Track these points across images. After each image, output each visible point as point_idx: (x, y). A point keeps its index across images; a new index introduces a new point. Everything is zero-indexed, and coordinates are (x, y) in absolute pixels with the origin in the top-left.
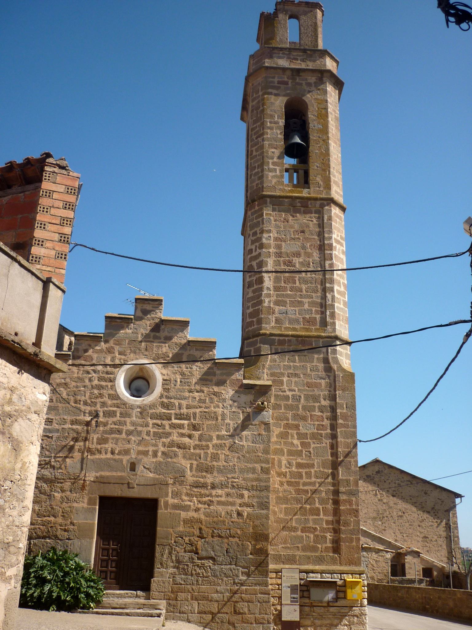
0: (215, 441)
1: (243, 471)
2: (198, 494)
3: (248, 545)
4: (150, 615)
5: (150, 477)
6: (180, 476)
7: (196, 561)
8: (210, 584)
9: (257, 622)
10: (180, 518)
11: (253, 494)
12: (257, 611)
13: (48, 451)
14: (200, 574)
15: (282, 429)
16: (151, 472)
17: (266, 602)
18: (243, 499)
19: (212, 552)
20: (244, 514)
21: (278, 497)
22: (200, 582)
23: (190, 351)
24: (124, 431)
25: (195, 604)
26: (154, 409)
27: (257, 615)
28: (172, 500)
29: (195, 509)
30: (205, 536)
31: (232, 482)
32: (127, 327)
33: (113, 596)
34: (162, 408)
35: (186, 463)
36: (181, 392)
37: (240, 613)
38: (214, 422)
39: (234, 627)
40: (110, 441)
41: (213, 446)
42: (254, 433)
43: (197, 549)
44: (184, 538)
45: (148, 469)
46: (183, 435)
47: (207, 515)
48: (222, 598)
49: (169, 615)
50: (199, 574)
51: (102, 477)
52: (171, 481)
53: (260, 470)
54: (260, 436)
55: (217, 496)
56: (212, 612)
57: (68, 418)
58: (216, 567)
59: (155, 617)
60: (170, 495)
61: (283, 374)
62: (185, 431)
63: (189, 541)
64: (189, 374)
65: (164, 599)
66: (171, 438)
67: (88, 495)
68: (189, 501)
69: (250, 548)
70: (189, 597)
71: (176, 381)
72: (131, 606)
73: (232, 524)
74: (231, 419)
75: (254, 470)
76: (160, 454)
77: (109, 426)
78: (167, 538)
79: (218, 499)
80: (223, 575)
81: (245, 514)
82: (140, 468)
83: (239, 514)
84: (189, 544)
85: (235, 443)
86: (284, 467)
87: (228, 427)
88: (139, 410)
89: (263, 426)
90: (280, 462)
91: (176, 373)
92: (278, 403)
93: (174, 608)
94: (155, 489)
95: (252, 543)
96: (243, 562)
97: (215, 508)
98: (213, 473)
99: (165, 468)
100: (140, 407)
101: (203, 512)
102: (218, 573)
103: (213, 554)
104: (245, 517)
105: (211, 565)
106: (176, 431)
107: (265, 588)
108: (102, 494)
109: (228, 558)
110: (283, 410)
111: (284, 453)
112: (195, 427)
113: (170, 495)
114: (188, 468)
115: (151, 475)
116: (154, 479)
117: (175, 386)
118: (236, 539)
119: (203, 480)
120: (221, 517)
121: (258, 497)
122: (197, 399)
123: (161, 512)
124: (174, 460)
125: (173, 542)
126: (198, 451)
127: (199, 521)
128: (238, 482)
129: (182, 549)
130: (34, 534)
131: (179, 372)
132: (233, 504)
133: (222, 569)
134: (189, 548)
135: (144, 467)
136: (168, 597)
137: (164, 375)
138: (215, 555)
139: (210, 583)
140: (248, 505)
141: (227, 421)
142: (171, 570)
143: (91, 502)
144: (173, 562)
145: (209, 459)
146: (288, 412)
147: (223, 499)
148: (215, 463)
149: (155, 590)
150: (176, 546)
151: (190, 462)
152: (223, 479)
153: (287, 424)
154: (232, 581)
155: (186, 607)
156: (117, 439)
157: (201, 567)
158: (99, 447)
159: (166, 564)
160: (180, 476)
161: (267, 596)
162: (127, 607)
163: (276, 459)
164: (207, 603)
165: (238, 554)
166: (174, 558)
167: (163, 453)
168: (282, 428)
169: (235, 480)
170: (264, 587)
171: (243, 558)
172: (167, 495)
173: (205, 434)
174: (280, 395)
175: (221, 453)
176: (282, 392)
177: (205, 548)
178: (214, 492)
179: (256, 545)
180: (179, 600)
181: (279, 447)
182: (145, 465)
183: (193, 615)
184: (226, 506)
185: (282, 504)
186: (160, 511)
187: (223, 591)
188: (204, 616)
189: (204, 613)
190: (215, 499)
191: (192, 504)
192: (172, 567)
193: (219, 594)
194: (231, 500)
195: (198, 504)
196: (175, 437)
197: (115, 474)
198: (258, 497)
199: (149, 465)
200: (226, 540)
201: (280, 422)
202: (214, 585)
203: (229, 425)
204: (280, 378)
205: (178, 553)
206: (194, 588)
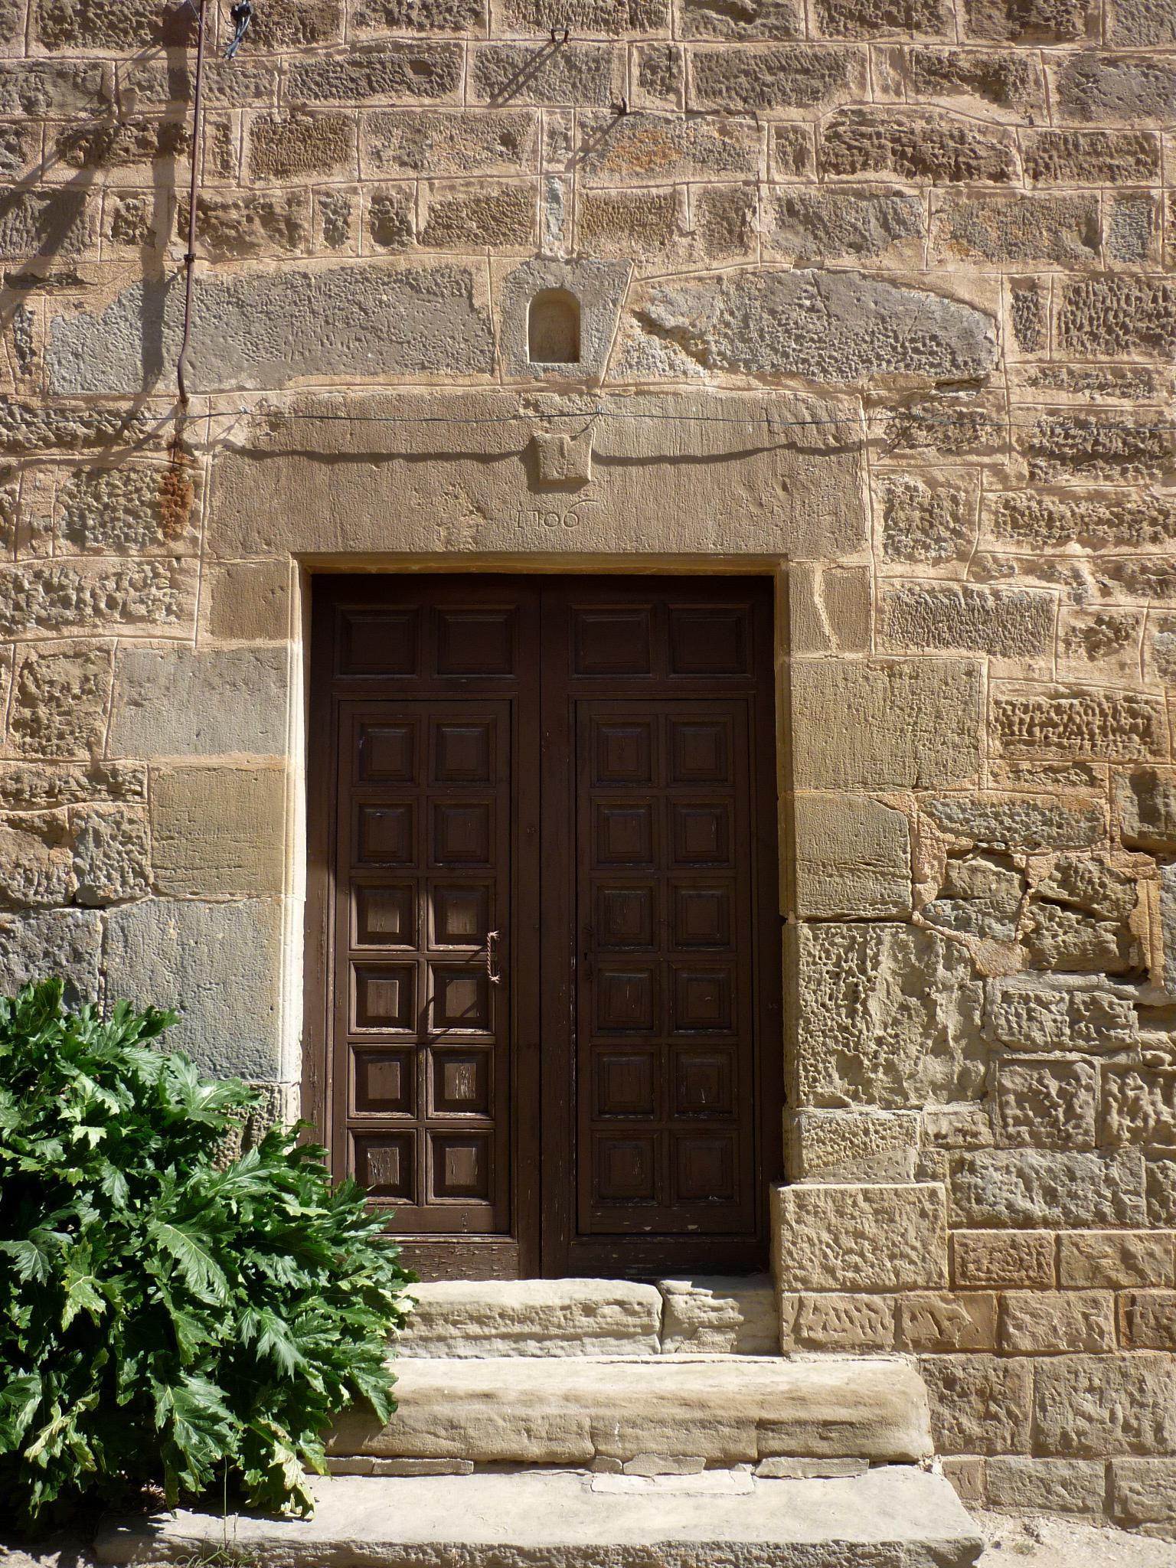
2: (1103, 512)
5: (703, 399)
6: (940, 385)
16: (702, 358)
33: (474, 1329)
52: (874, 426)
63: (1064, 883)
65: (899, 1346)
68: (1030, 569)
114: (1005, 316)
115: (711, 383)
116: (735, 411)
125: (929, 891)
135: (651, 325)
150: (963, 924)
160: (940, 385)
162: (615, 1448)
166: (949, 1018)
172: (852, 535)
191: (1058, 591)
205: (978, 975)
206: (1137, 1248)
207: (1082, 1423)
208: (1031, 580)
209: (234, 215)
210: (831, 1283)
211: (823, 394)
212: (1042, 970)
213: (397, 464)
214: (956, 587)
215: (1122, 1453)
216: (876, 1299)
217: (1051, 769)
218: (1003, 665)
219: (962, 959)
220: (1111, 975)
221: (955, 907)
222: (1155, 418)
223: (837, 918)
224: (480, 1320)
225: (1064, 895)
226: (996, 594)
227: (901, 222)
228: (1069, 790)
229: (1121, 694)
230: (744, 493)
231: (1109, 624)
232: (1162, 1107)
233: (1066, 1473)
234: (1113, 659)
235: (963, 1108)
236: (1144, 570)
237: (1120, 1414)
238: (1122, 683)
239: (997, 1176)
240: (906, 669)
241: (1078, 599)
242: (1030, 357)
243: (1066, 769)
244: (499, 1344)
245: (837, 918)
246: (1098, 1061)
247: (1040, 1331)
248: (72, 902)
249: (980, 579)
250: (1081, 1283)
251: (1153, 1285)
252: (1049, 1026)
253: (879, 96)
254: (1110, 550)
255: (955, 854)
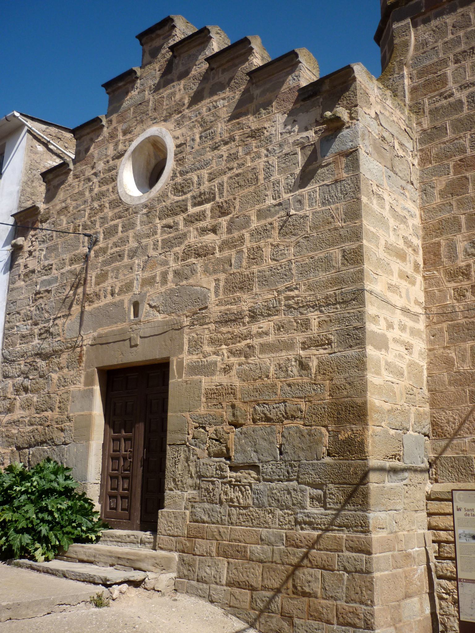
0: (255, 224)
1: (307, 269)
2: (230, 336)
3: (321, 433)
4: (91, 580)
5: (159, 321)
6: (200, 310)
7: (229, 473)
8: (252, 523)
9: (341, 620)
10: (200, 389)
11: (329, 316)
12: (342, 593)
13: (48, 312)
14: (233, 502)
15: (451, 176)
16: (159, 311)
17: (361, 572)
18: (309, 332)
19: (253, 454)
20: (311, 364)
21: (453, 326)
22: (234, 518)
23: (213, 78)
24: (126, 252)
25: (223, 563)
26: (164, 201)
27: (341, 603)
28: (190, 357)
29: (225, 368)
30: (241, 421)
31: (288, 298)
32: (133, 88)
33: (111, 539)
34: (175, 195)
35: (209, 282)
36: (201, 155)
37: (305, 594)
38: (252, 189)
39: (292, 625)
40: (110, 274)
41: (252, 235)
42: (326, 182)
43: (228, 449)
44: (207, 429)
45: (154, 307)
46: (203, 231)
47: (243, 376)
48: (270, 555)
49: (181, 583)
50: (232, 500)
51: (100, 336)
52: (186, 322)
53: (340, 258)
54: (338, 184)
55: (260, 335)
56: (252, 586)
57: (67, 257)
58: (261, 486)
59: (98, 584)
60: (186, 347)
61: (444, 62)
62: (207, 223)
63: (216, 435)
64: (213, 119)
65: (176, 551)
66: (186, 242)
67: (85, 370)
68: (214, 353)
69: (326, 440)
70: (214, 549)
71: (193, 140)
72: (102, 559)
73: (289, 388)
74: (281, 171)
75: (327, 262)
76: (170, 276)
77: (110, 251)
78: (181, 431)
79: (261, 340)
80: (274, 504)
81: (314, 364)
82: (145, 308)
83: (303, 366)
84: (216, 440)
85: (289, 215)
86: (461, 256)
87: (276, 188)
88: (145, 211)
89: (344, 160)
90: (452, 247)
91: (194, 126)
92: (438, 124)
93: (189, 570)
94: (165, 342)
95: (330, 428)
96: (312, 473)
97: (257, 361)
98: (252, 289)
99: (178, 299)
100: (146, 206)
101: (237, 373)
102: (265, 500)
103: (254, 458)
104: (313, 371)
105: (253, 481)
106: (195, 226)
107: (362, 535)
108: (101, 365)
109: (283, 467)
110: (450, 135)
111: (460, 226)
112: (222, 210)
113: (186, 347)
114: (213, 290)
115: (160, 317)
116: (166, 323)
117: (193, 148)
118: (299, 423)
119: (234, 307)
120: (267, 377)
121: (339, 321)
122: (225, 155)
123: (174, 381)
124: (191, 281)
125: (190, 437)
126: (226, 253)
127: (230, 391)
128: (298, 296)
129: (204, 450)
130: (33, 440)
131: (199, 122)
132: (289, 346)
133: (272, 489)
134: (216, 447)
135: (151, 306)
136: (180, 547)
137: (178, 138)
138: (259, 460)
139: (252, 520)
140: (319, 344)
141: (276, 176)
142: (190, 493)
143: (89, 382)
144: (192, 477)
145: (244, 264)
146: (462, 134)
147: (271, 338)
148: (255, 269)
149: (164, 532)
150: (196, 445)
151: (215, 277)
152: (270, 296)
153: (461, 160)
154: (292, 518)
155: (208, 570)
156: (117, 269)
157: (235, 485)
158: (97, 289)
159: (182, 481)
160: (200, 310)
161: (364, 556)
162: (97, 560)
163: (443, 243)
164: (243, 564)
165: (302, 454)
166: (193, 470)
167: (176, 273)
168: (452, 174)
169: (292, 294)
170: (358, 535)
171: (313, 465)
172: (181, 350)
173: (237, 217)
174: (442, 107)
175: (265, 245)
176: (445, 98)
177: (240, 445)
178: (254, 328)
179: (339, 432)
180: (198, 553)
181: (447, 215)
182: (151, 302)
183: (219, 587)
184: (277, 352)
185: (464, 341)
186: (171, 381)
187: (273, 539)
188: (236, 591)
189: (237, 585)
190: (256, 342)
191: (219, 359)
192: (191, 487)
193: (265, 547)
194: (284, 337)
195: (228, 357)
196: (193, 239)
197: (115, 328)
198: (339, 321)
199: (155, 299)
200: (278, 427)
201: (446, 162)
202: (259, 526)
203: (278, 183)
204: (439, 73)
205: (198, 458)
206: (221, 530)
207: (205, 574)
208: (215, 356)
209: (92, 295)
210: (165, 534)
211: (179, 316)
212: (211, 457)
213: (111, 344)
214: (199, 360)
215: (213, 583)
216: (173, 538)
217: (214, 405)
218: (208, 379)
219: (195, 455)
220: (225, 458)
221: (195, 441)
222: (240, 309)
223: (173, 445)
224: (112, 537)
225: (216, 437)
226: (207, 361)
227: (194, 270)
228: (218, 410)
229: (229, 384)
230: (163, 343)
231: (228, 366)
232: (233, 493)
233: (201, 587)
234: (228, 375)
235: (195, 492)
236: (237, 351)
237: (213, 573)
238: (230, 381)
239: (199, 510)
240: (189, 382)
241: (222, 360)
242: (217, 299)
243: (217, 405)
244: (115, 543)
245: (173, 445)
246: (220, 481)
247: (201, 550)
248: (63, 444)
249: (204, 358)
250: (211, 538)
251: (225, 541)
252: (211, 471)
253: (194, 240)
254: (231, 346)
255: (196, 428)
